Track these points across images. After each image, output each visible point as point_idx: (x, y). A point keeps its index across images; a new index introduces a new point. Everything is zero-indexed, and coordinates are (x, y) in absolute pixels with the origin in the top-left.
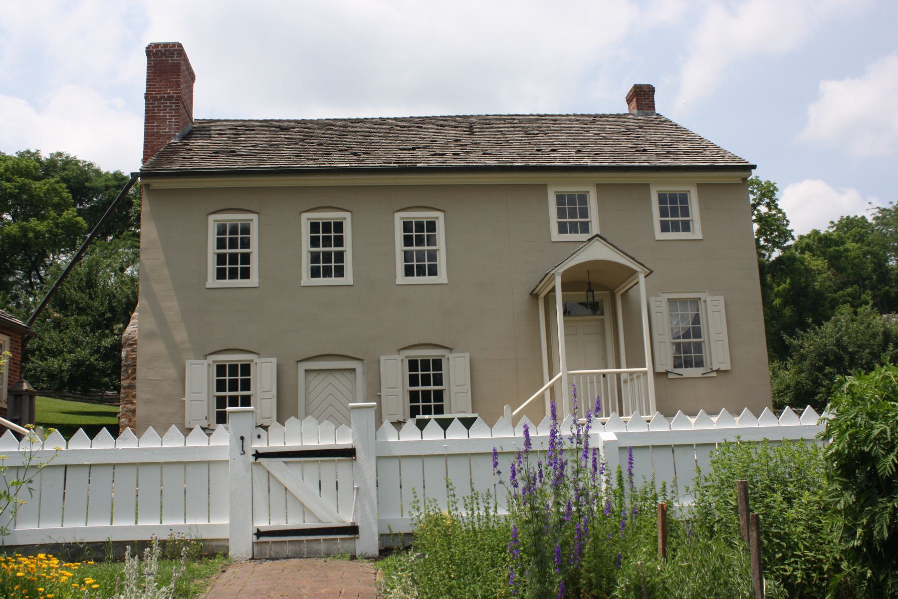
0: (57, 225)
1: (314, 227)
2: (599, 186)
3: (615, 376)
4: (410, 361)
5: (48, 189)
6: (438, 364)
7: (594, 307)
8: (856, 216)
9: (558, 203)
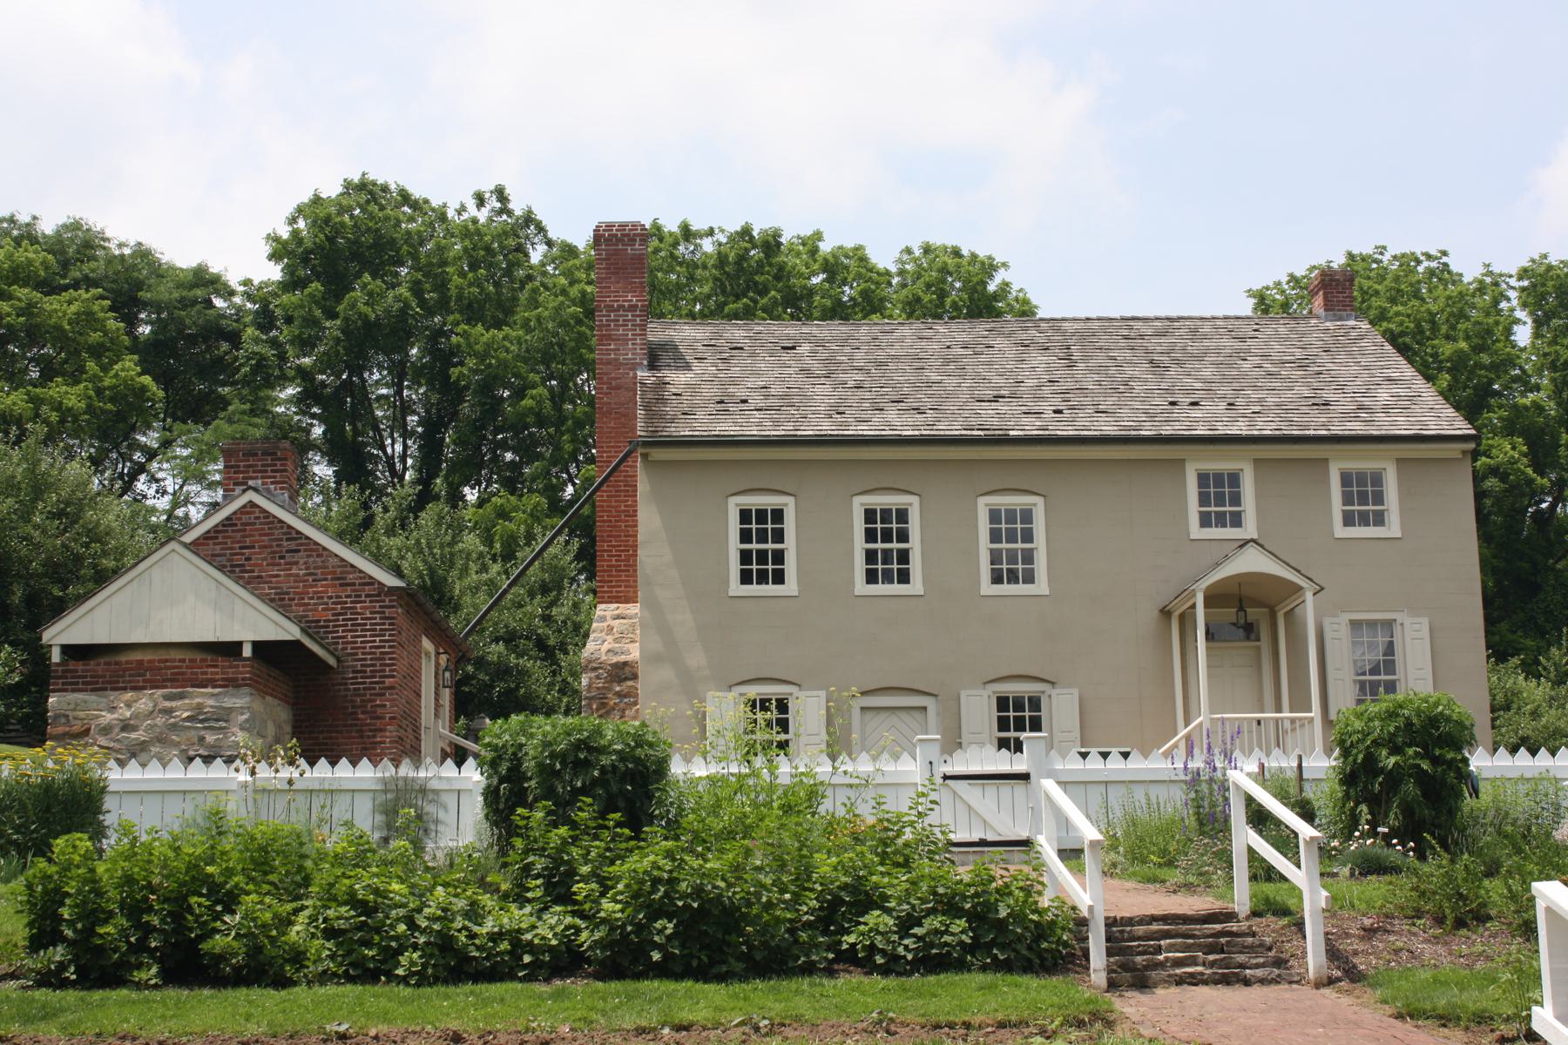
0: (99, 392)
6: (1035, 703)
7: (1249, 630)
9: (1200, 486)
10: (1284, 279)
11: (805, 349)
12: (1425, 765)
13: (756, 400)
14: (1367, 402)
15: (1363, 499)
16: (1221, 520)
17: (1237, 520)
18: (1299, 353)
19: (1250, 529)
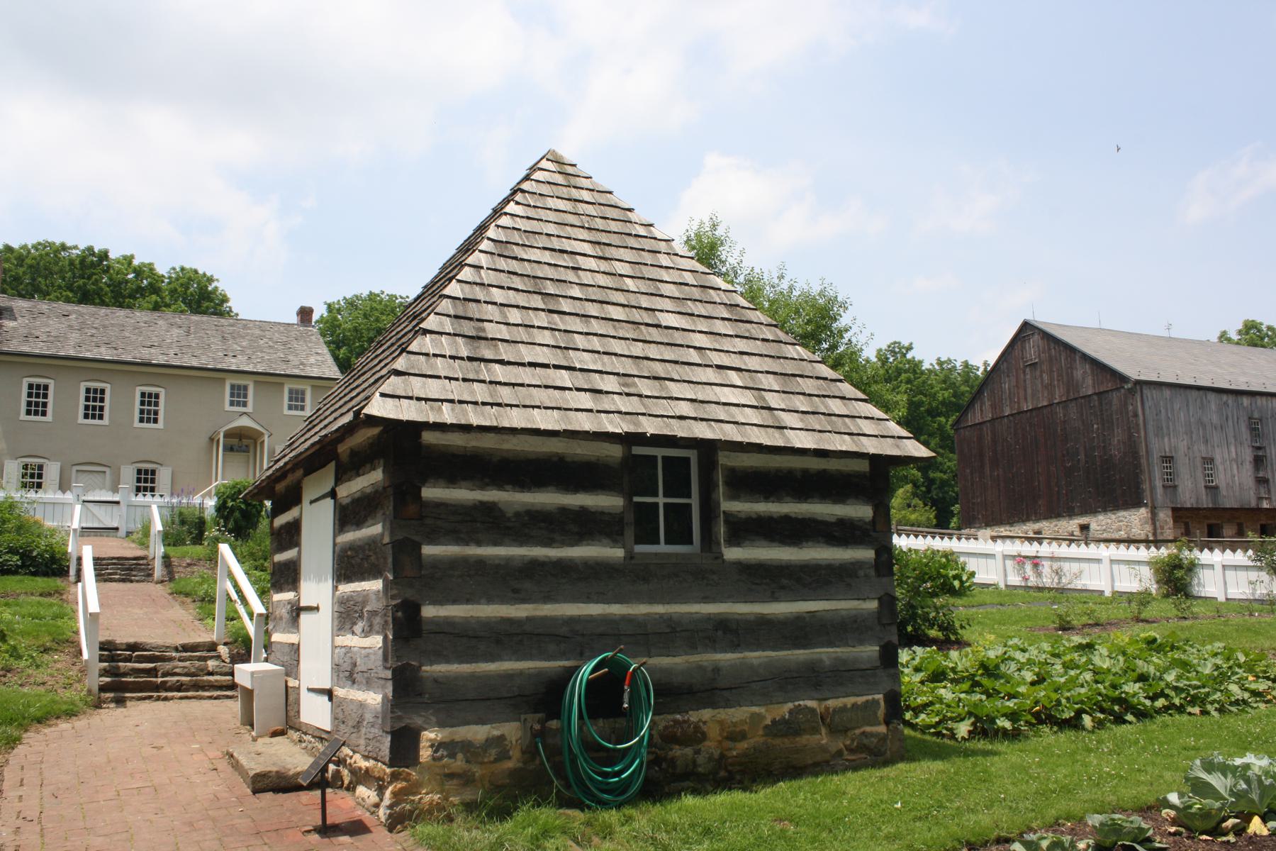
1: (88, 390)
6: (153, 472)
10: (341, 299)
11: (73, 317)
12: (243, 506)
13: (43, 337)
14: (305, 361)
15: (297, 400)
16: (238, 404)
17: (245, 404)
18: (285, 339)
19: (249, 409)
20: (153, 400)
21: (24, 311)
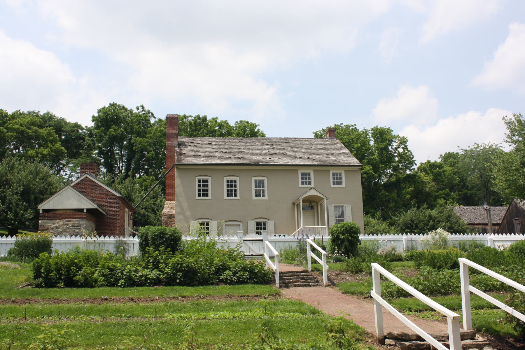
0: (52, 151)
1: (228, 181)
2: (314, 170)
3: (317, 229)
4: (256, 223)
5: (47, 133)
6: (264, 224)
7: (312, 208)
8: (454, 152)
9: (302, 175)
10: (321, 130)
11: (213, 144)
13: (202, 155)
14: (338, 157)
18: (323, 146)
19: (312, 185)
20: (205, 193)
21: (190, 142)
